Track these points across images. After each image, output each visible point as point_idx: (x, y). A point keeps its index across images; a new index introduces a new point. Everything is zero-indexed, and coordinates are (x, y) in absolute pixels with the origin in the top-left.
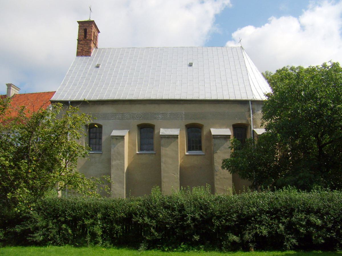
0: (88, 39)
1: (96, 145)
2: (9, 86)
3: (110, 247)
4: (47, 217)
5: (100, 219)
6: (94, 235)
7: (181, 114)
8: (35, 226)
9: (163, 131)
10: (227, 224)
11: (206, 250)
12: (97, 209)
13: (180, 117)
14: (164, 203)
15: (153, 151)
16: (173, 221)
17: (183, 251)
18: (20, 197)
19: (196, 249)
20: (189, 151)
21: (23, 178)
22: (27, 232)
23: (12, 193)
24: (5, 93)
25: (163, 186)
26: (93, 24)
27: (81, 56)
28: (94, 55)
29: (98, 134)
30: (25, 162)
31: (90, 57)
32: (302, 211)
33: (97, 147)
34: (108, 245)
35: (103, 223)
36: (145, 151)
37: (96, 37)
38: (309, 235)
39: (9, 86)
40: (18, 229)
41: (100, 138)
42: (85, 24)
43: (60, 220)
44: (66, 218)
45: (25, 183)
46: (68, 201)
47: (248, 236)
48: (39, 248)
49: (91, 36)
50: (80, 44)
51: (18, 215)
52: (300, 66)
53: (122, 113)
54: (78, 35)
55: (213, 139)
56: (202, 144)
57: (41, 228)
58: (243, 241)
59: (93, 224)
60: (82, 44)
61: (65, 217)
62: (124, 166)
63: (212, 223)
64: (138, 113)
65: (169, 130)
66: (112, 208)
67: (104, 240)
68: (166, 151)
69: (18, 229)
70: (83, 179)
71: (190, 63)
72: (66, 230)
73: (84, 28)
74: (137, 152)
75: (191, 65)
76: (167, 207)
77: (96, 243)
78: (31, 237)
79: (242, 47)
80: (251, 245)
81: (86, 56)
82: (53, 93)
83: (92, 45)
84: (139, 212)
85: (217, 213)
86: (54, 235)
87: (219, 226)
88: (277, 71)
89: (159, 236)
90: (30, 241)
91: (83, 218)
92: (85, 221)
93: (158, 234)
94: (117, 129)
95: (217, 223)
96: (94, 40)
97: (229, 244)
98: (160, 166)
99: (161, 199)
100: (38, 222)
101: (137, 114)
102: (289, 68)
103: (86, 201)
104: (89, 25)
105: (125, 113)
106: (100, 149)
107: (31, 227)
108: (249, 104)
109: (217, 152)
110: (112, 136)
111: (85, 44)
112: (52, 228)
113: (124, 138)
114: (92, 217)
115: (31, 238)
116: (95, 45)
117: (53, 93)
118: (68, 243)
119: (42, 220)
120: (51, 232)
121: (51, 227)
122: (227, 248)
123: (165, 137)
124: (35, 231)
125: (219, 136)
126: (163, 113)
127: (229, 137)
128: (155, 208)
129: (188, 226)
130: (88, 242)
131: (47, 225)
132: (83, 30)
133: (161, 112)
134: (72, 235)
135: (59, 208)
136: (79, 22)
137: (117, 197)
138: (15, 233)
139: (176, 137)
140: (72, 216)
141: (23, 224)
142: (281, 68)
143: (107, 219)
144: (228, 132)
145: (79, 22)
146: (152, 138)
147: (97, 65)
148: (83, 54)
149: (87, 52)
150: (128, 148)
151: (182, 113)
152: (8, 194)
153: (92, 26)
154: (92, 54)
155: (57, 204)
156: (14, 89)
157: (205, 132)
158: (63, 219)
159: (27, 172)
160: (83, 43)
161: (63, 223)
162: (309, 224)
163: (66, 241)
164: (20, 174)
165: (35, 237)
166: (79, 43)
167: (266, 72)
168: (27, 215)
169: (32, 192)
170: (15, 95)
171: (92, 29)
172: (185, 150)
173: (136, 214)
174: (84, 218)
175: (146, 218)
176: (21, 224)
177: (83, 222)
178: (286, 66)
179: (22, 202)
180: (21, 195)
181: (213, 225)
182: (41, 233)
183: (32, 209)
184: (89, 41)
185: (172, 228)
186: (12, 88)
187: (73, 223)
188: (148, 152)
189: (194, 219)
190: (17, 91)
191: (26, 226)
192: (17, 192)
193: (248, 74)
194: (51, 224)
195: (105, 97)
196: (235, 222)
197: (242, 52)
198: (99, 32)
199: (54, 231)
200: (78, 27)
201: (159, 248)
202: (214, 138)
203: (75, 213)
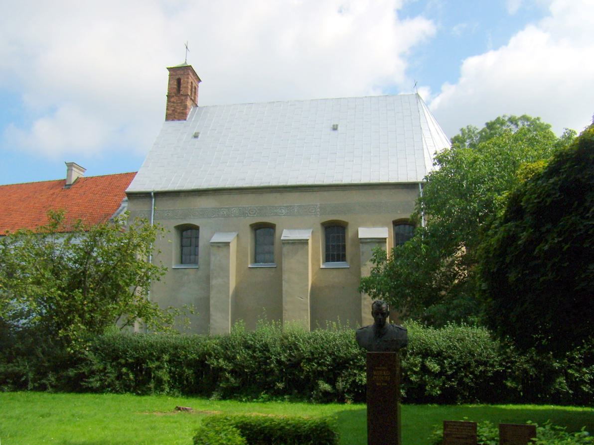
0: (182, 95)
1: (190, 255)
2: (70, 166)
3: (177, 396)
4: (105, 358)
5: (166, 361)
6: (159, 382)
7: (315, 206)
8: (90, 369)
9: (287, 234)
10: (319, 368)
11: (291, 401)
12: (164, 348)
13: (313, 211)
14: (246, 342)
15: (273, 262)
16: (255, 365)
17: (263, 402)
18: (74, 335)
19: (281, 400)
20: (326, 262)
21: (77, 311)
22: (82, 376)
23: (66, 330)
24: (63, 176)
25: (285, 315)
26: (189, 71)
27: (173, 120)
28: (191, 118)
29: (193, 240)
30: (79, 292)
31: (185, 121)
32: (418, 354)
33: (192, 257)
34: (176, 394)
35: (171, 367)
36: (261, 263)
37: (195, 88)
38: (422, 386)
39: (70, 166)
40: (71, 372)
41: (197, 246)
42: (179, 72)
43: (120, 363)
44: (127, 360)
45: (80, 317)
46: (131, 339)
47: (340, 385)
48: (94, 395)
49: (187, 89)
50: (170, 101)
51: (71, 356)
52: (524, 114)
53: (227, 208)
54: (168, 88)
55: (361, 245)
56: (346, 251)
57: (97, 372)
58: (338, 390)
59: (159, 368)
60: (174, 102)
61: (125, 359)
62: (229, 288)
63: (301, 367)
64: (251, 207)
65: (297, 231)
66: (184, 348)
67: (172, 387)
68: (290, 263)
69: (71, 372)
70: (155, 310)
71: (334, 125)
72: (127, 374)
73: (177, 77)
74: (250, 266)
75: (335, 128)
76: (248, 347)
77: (163, 390)
78: (85, 382)
79: (417, 94)
80: (347, 396)
81: (179, 120)
82: (131, 176)
83: (189, 103)
84: (214, 352)
85: (307, 355)
86: (112, 381)
87: (309, 372)
88: (487, 124)
89: (236, 383)
90: (84, 387)
91: (148, 361)
92: (149, 363)
93: (234, 381)
94: (219, 231)
95: (306, 368)
96: (191, 94)
97: (320, 394)
98: (281, 285)
99: (243, 337)
100: (93, 365)
101: (249, 208)
102: (506, 119)
103: (152, 340)
104: (184, 72)
105: (232, 208)
106: (196, 262)
107: (85, 370)
108: (419, 188)
109: (366, 263)
110: (212, 243)
111: (178, 102)
112: (111, 373)
113: (229, 245)
114: (158, 359)
115: (86, 384)
116: (194, 101)
117: (131, 176)
118: (129, 391)
119: (99, 362)
120: (108, 377)
121: (109, 371)
122: (318, 400)
123: (288, 243)
124: (91, 376)
125: (368, 240)
126: (287, 207)
127: (384, 240)
128: (234, 348)
129: (272, 370)
130: (153, 390)
131: (105, 368)
132: (176, 81)
133: (285, 205)
134: (134, 380)
135: (119, 348)
136: (170, 69)
137: (221, 334)
138: (69, 378)
139: (305, 242)
140: (134, 358)
141: (77, 367)
142: (493, 119)
143: (177, 361)
144: (384, 232)
145: (170, 69)
146: (273, 244)
147: (196, 133)
148: (175, 118)
149: (181, 114)
150: (235, 259)
151: (317, 205)
152: (60, 332)
153: (189, 74)
154: (188, 116)
155: (117, 343)
156: (77, 170)
157: (350, 234)
158: (123, 361)
159: (83, 304)
160: (175, 101)
161: (124, 366)
162: (425, 369)
163: (127, 388)
164: (74, 306)
165: (90, 382)
166: (169, 101)
167: (468, 126)
168: (82, 356)
169: (90, 328)
170: (78, 180)
171: (188, 78)
172: (320, 261)
173: (210, 355)
174: (149, 360)
175: (221, 360)
176: (75, 367)
177: (148, 365)
178: (501, 116)
179: (76, 340)
180: (75, 333)
181: (302, 370)
182: (98, 378)
183: (87, 349)
184: (183, 98)
185: (252, 373)
186: (74, 169)
187: (137, 366)
188: (261, 265)
189: (279, 362)
190: (82, 173)
191: (81, 369)
192: (70, 329)
193: (423, 139)
194: (109, 367)
195: (204, 185)
196: (329, 365)
197: (417, 103)
198: (199, 81)
199: (113, 376)
200: (168, 77)
201: (235, 398)
202: (362, 243)
203: (138, 354)
